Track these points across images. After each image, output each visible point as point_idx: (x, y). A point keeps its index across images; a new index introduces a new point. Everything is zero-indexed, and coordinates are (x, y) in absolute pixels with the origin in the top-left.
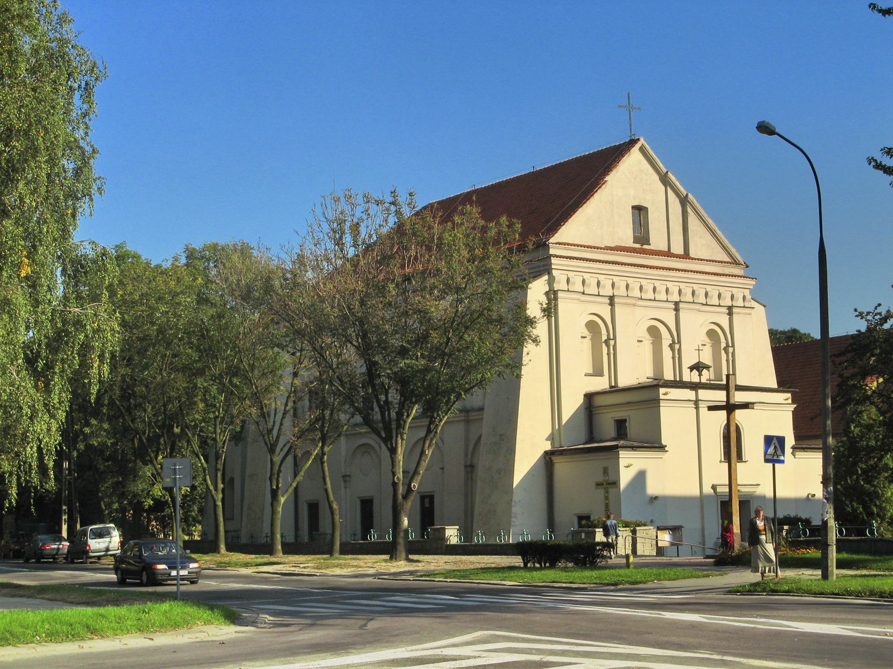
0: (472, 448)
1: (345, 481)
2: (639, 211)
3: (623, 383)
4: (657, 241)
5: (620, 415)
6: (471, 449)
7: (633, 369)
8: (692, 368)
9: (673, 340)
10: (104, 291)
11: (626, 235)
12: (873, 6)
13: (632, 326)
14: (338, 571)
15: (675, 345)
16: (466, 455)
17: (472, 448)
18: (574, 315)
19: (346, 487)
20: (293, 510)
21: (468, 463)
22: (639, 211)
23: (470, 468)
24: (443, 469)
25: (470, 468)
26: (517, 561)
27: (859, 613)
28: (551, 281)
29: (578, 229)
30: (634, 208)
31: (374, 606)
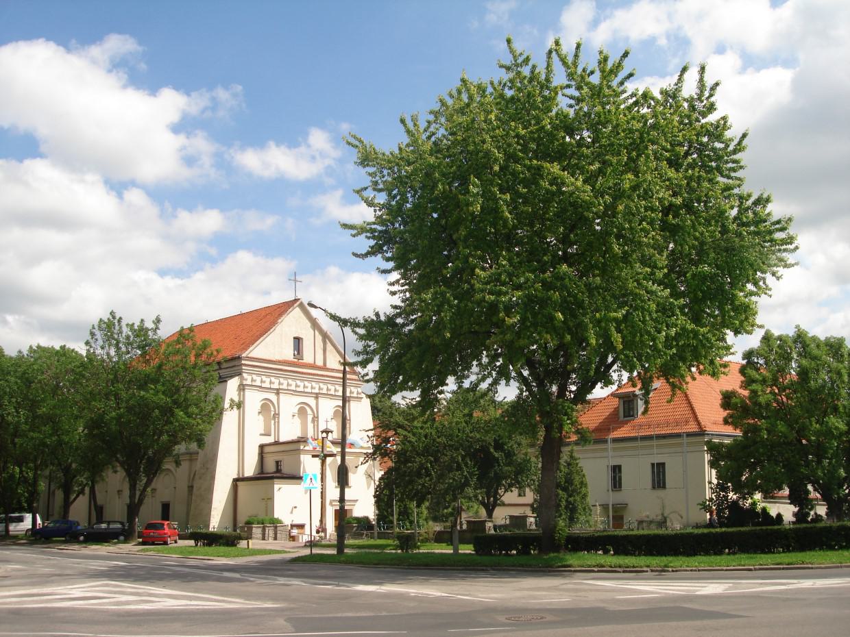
0: (192, 477)
1: (119, 494)
2: (298, 341)
3: (282, 440)
4: (308, 357)
5: (278, 458)
6: (192, 476)
7: (289, 430)
8: (322, 432)
9: (314, 415)
10: (420, 248)
11: (288, 353)
12: (355, 255)
13: (288, 405)
14: (376, 551)
15: (315, 419)
16: (189, 482)
17: (192, 477)
18: (253, 400)
19: (119, 498)
20: (88, 510)
21: (190, 485)
22: (298, 341)
23: (191, 488)
24: (106, 492)
25: (191, 488)
26: (192, 542)
27: (636, 571)
28: (242, 379)
29: (260, 350)
30: (294, 338)
31: (695, 586)
